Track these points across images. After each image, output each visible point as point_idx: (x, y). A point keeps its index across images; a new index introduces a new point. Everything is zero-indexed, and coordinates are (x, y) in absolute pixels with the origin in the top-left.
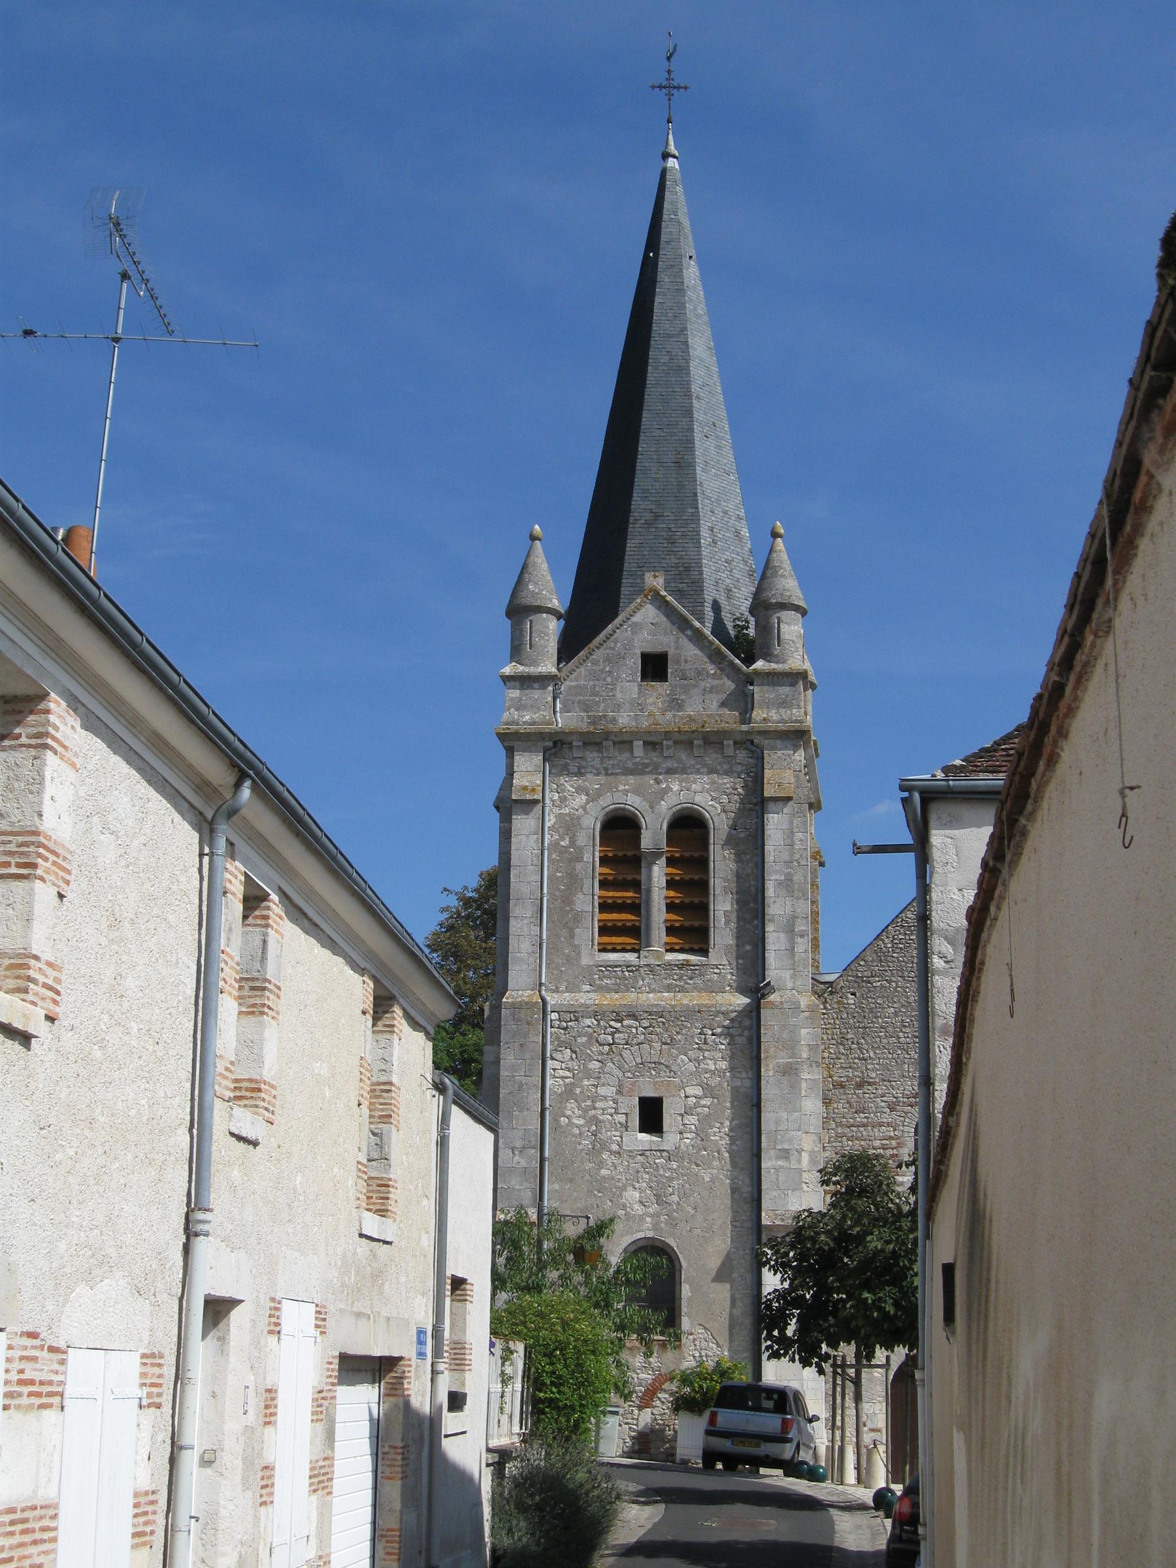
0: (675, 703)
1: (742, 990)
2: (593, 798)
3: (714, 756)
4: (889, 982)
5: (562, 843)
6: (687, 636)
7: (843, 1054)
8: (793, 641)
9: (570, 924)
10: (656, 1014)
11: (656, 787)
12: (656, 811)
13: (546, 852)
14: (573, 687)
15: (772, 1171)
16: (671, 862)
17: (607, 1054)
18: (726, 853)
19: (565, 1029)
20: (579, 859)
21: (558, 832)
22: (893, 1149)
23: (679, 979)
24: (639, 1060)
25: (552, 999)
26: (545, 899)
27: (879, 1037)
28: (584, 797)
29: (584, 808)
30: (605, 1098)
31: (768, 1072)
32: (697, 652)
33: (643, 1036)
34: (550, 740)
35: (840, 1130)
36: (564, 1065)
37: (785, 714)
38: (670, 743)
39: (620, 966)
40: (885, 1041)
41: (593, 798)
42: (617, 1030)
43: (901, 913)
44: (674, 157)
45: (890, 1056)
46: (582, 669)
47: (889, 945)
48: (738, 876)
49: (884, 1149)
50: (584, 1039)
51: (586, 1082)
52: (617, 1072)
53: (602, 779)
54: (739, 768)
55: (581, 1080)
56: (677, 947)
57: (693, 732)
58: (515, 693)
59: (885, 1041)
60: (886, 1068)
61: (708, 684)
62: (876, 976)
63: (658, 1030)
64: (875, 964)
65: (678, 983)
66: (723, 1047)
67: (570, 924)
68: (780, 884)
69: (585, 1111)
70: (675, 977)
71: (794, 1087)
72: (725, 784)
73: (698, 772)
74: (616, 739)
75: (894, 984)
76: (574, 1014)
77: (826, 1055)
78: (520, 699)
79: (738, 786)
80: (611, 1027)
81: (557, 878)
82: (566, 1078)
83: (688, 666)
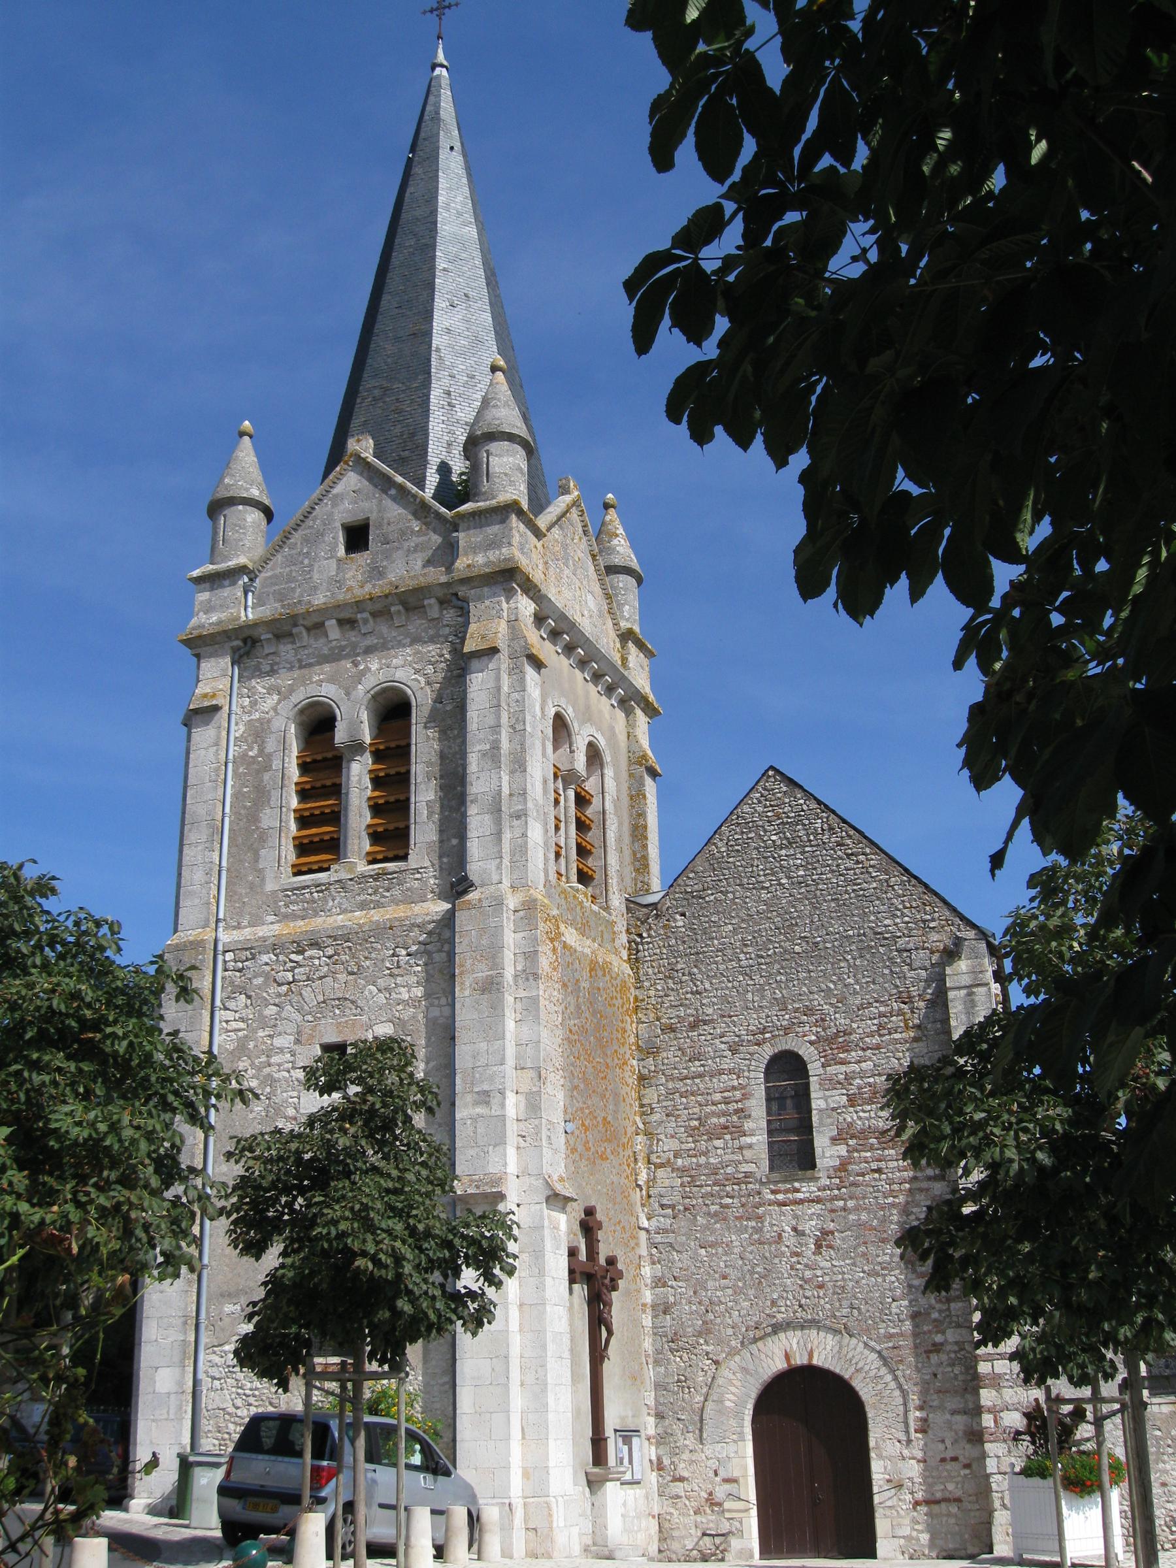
0: (376, 572)
1: (443, 896)
2: (284, 697)
3: (418, 622)
4: (725, 893)
5: (251, 754)
6: (391, 497)
7: (673, 990)
8: (506, 474)
9: (255, 845)
10: (343, 937)
11: (354, 670)
12: (352, 698)
13: (230, 766)
14: (270, 577)
15: (469, 1122)
16: (378, 756)
17: (285, 995)
18: (430, 732)
19: (240, 971)
20: (267, 767)
21: (246, 741)
22: (736, 1102)
23: (375, 893)
24: (321, 998)
25: (225, 937)
26: (227, 820)
27: (716, 963)
28: (276, 697)
29: (275, 709)
30: (281, 1050)
31: (464, 991)
32: (401, 511)
33: (326, 968)
34: (237, 639)
35: (670, 1085)
36: (237, 1015)
37: (493, 555)
38: (366, 615)
39: (308, 887)
40: (722, 967)
41: (284, 697)
42: (299, 965)
43: (736, 808)
44: (442, 66)
45: (730, 985)
46: (279, 557)
47: (723, 849)
48: (442, 756)
49: (727, 1103)
50: (260, 980)
51: (261, 1033)
52: (297, 1017)
53: (296, 673)
54: (447, 630)
55: (255, 1031)
56: (380, 857)
57: (386, 596)
58: (203, 596)
59: (722, 967)
60: (725, 999)
61: (416, 540)
62: (708, 888)
63: (343, 958)
64: (707, 874)
65: (373, 897)
66: (419, 968)
67: (255, 845)
68: (484, 754)
69: (259, 1069)
70: (370, 891)
71: (497, 1008)
72: (429, 652)
73: (401, 645)
74: (308, 623)
75: (730, 896)
76: (250, 950)
77: (652, 993)
78: (209, 601)
79: (445, 652)
80: (291, 961)
81: (243, 794)
82: (240, 1030)
83: (391, 529)
